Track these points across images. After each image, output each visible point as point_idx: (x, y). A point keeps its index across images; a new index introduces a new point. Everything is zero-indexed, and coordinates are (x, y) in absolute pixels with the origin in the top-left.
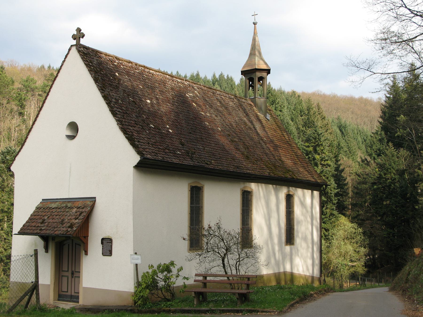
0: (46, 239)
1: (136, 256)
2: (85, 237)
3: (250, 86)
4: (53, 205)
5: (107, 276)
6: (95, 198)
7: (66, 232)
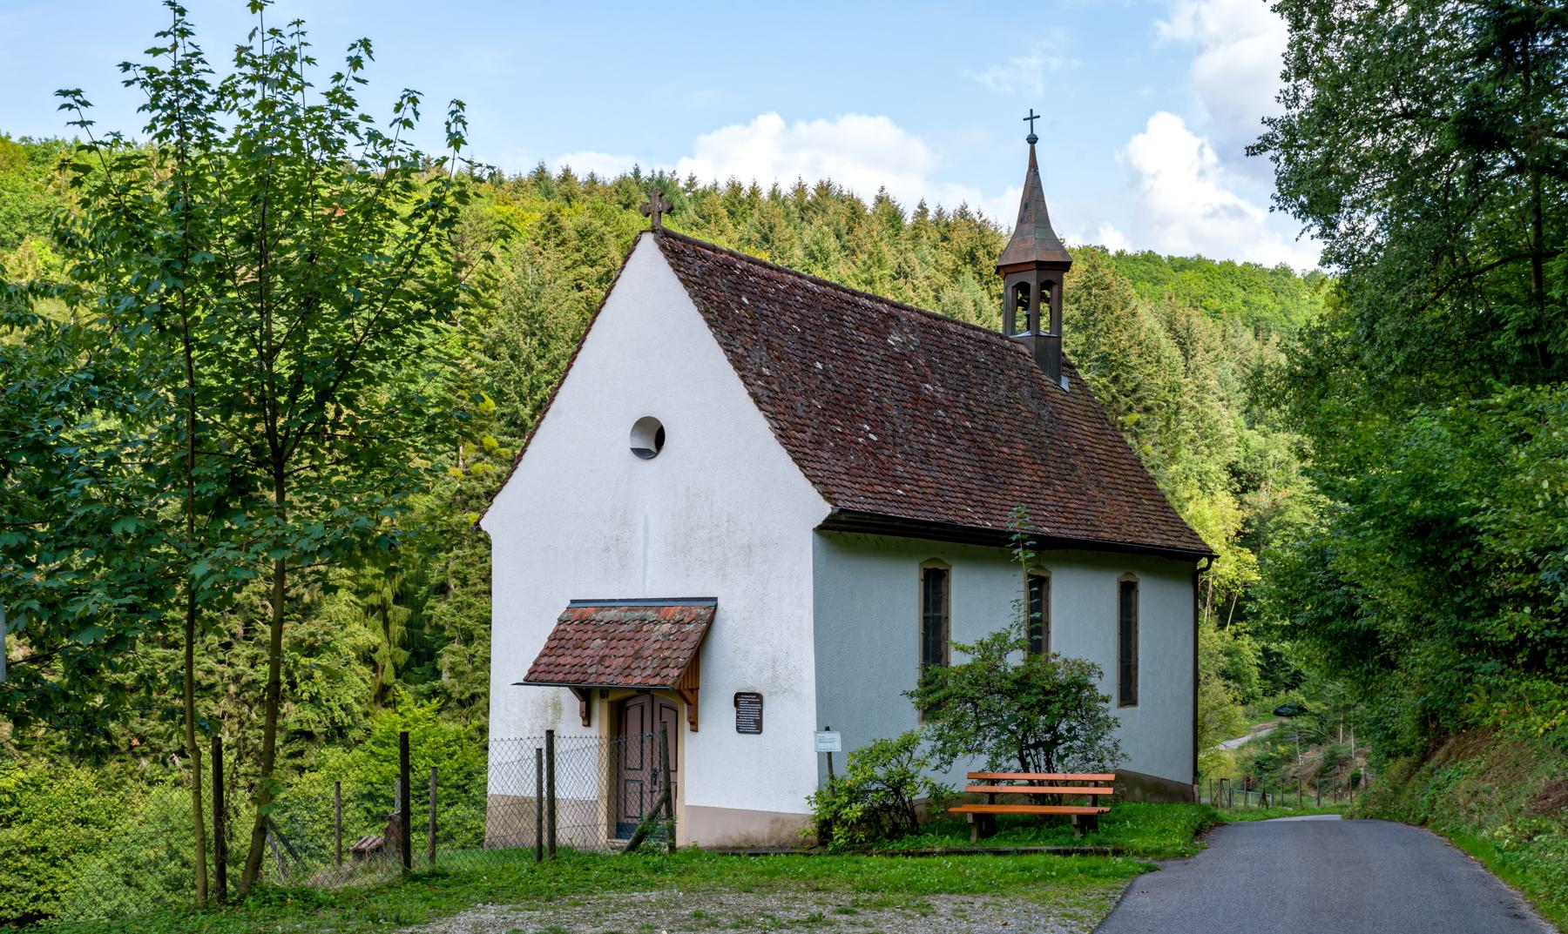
0: (585, 694)
1: (827, 735)
2: (692, 690)
3: (1020, 303)
4: (611, 614)
5: (747, 777)
6: (715, 599)
7: (642, 681)
